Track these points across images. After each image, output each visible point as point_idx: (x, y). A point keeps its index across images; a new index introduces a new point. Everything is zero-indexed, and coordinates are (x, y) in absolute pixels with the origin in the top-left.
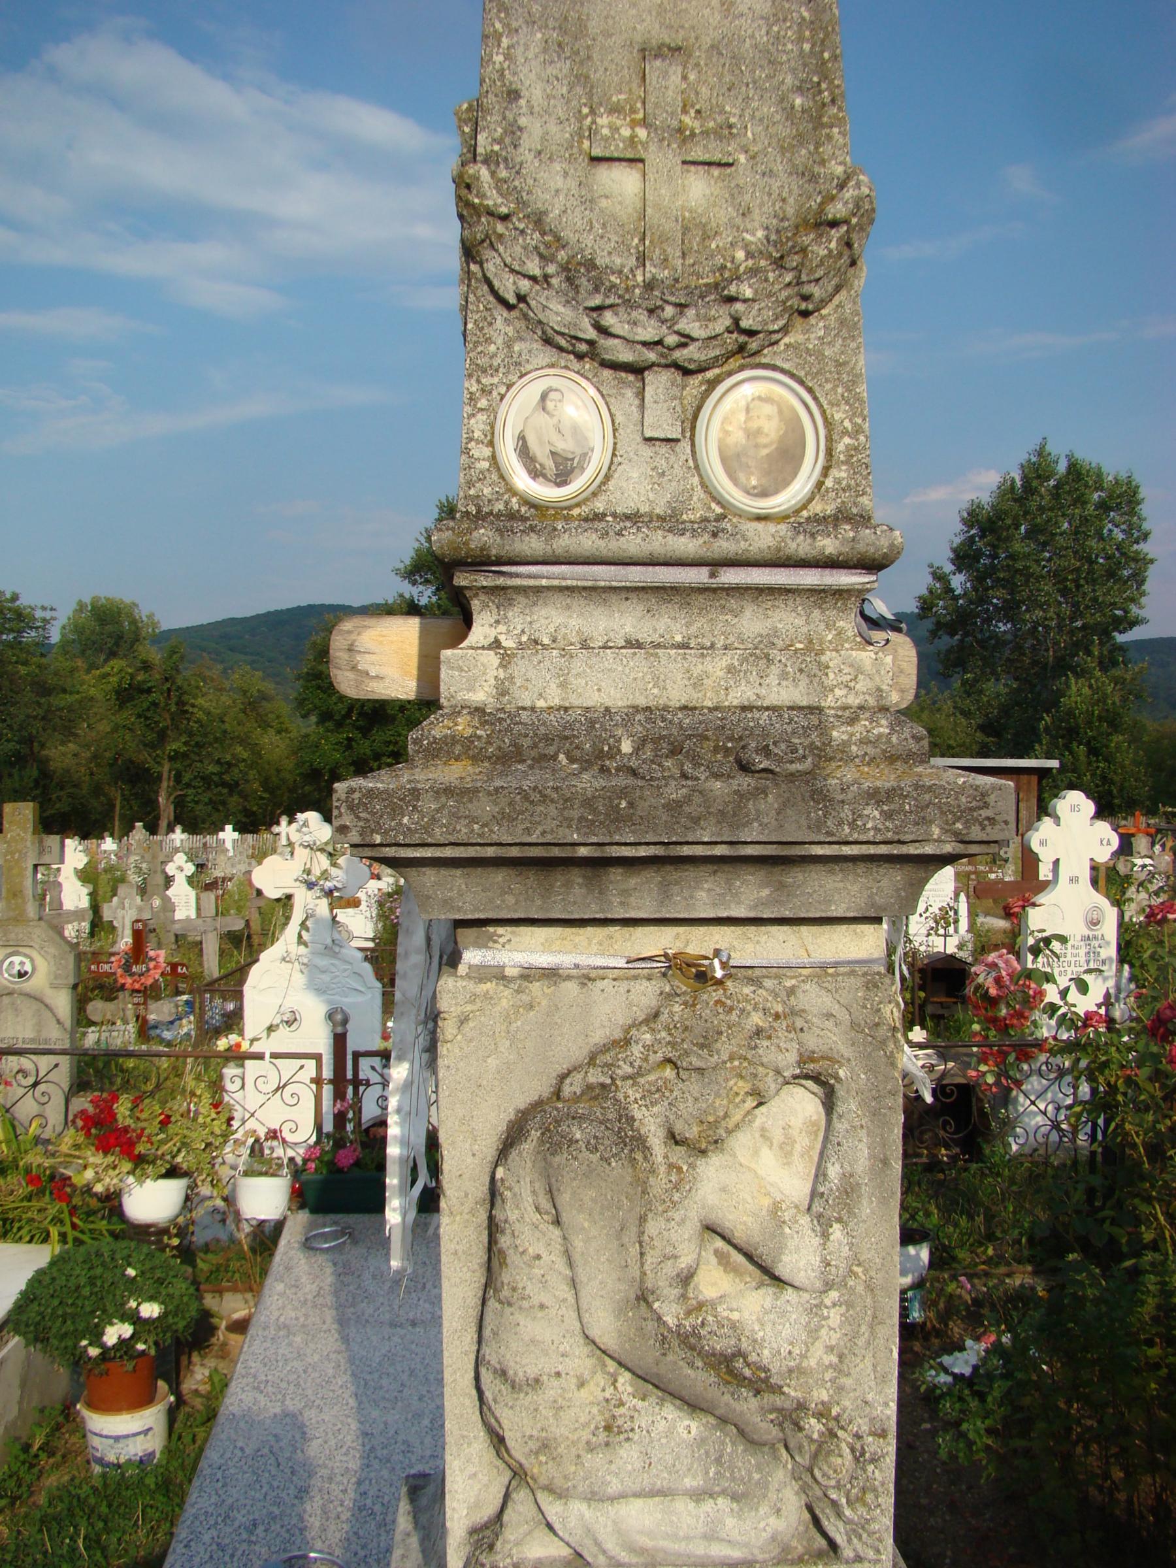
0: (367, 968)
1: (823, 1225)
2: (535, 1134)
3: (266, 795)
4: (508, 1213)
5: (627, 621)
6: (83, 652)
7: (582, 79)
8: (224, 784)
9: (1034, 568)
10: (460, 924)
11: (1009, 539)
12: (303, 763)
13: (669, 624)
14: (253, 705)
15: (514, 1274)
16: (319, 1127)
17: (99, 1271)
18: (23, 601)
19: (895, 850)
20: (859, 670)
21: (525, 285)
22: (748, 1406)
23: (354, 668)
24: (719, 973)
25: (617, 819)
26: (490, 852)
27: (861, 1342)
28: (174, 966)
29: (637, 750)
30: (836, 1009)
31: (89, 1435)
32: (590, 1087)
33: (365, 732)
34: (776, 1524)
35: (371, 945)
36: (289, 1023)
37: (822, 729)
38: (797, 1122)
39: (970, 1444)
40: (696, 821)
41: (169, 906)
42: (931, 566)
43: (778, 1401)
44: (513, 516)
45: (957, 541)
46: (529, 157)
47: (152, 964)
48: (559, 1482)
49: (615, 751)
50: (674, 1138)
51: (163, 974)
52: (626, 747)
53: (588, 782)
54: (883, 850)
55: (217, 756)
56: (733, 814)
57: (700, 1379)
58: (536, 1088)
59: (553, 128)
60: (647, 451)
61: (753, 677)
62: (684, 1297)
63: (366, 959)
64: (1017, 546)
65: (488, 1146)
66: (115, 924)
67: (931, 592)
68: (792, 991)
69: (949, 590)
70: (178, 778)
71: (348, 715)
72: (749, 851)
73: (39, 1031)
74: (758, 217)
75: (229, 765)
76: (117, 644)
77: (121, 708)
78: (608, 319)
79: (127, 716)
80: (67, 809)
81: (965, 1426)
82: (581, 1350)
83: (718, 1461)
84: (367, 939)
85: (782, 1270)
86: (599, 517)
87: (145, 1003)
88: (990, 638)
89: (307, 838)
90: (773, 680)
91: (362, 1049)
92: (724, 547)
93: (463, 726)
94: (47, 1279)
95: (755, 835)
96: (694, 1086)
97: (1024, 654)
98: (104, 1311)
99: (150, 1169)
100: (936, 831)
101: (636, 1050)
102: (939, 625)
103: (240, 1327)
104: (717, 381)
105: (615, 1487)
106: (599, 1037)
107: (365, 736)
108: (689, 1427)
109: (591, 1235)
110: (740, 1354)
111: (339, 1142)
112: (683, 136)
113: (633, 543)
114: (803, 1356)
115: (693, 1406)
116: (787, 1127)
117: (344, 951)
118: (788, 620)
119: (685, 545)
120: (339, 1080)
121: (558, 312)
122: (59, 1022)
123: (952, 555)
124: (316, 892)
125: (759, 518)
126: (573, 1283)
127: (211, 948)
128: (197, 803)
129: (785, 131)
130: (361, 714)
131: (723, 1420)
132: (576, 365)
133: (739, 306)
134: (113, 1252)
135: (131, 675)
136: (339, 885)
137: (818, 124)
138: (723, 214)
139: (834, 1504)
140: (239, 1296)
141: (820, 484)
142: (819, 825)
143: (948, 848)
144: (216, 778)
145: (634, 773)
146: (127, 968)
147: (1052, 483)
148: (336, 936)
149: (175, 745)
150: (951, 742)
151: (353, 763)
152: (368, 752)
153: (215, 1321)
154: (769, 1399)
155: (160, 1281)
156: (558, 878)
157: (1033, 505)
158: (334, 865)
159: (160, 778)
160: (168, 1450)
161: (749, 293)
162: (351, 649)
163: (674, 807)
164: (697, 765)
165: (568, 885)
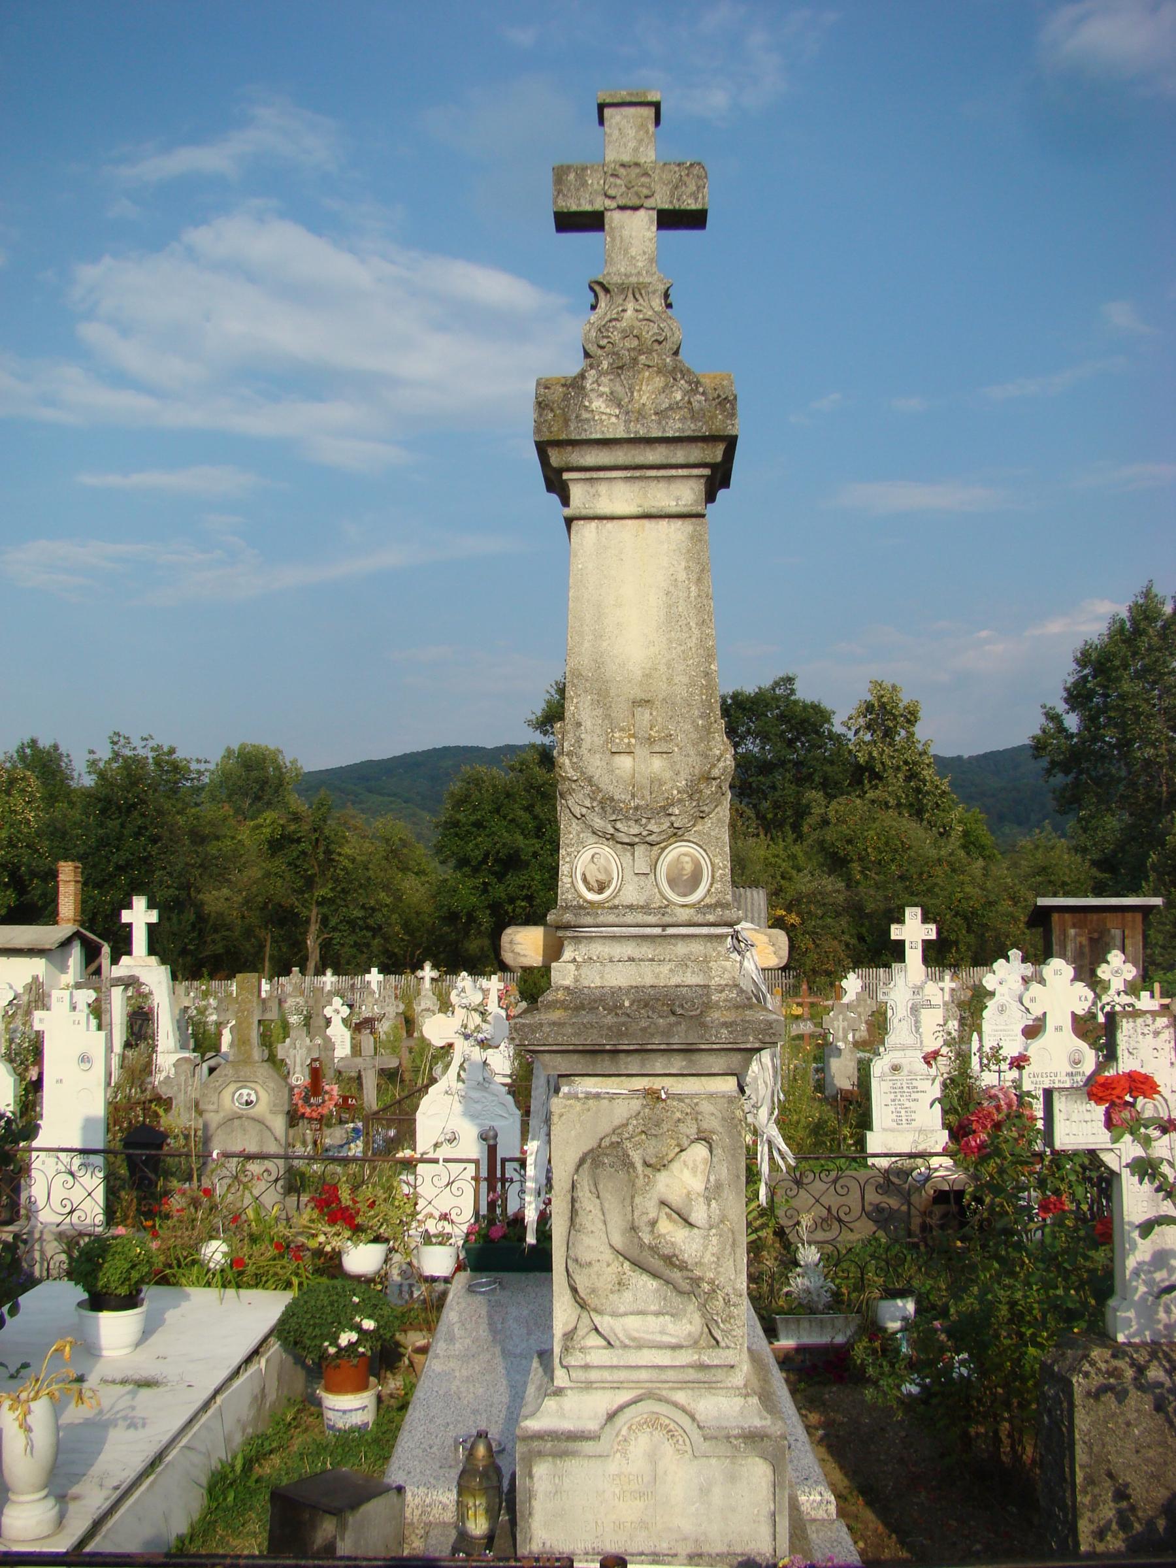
0: (510, 1098)
1: (708, 1200)
2: (589, 1161)
3: (406, 938)
4: (579, 1194)
5: (629, 949)
6: (230, 796)
7: (608, 716)
8: (368, 928)
9: (1144, 707)
10: (560, 1076)
11: (1119, 679)
12: (443, 906)
13: (647, 950)
14: (395, 855)
15: (581, 1219)
16: (476, 1213)
17: (335, 1297)
18: (179, 755)
19: (735, 1046)
20: (725, 970)
21: (584, 811)
22: (676, 1275)
23: (513, 951)
24: (664, 1096)
25: (620, 1034)
26: (571, 1048)
27: (727, 1252)
28: (345, 1099)
29: (631, 1004)
30: (715, 1112)
31: (325, 1411)
32: (612, 1143)
33: (500, 877)
34: (689, 1327)
35: (508, 1080)
36: (450, 1141)
37: (708, 995)
38: (699, 1159)
39: (885, 1394)
40: (652, 1035)
41: (329, 1045)
42: (1043, 707)
43: (690, 1274)
44: (581, 907)
45: (1071, 680)
46: (586, 752)
47: (327, 1097)
48: (599, 1306)
49: (622, 1006)
50: (646, 1164)
51: (336, 1105)
52: (627, 1004)
53: (610, 1020)
54: (730, 1046)
55: (362, 901)
56: (668, 1032)
57: (656, 1263)
58: (590, 1144)
59: (596, 739)
60: (636, 879)
61: (681, 973)
62: (652, 1232)
63: (509, 1093)
64: (1126, 687)
65: (571, 1167)
66: (287, 1061)
67: (1044, 732)
68: (697, 1104)
69: (1061, 729)
70: (325, 921)
71: (484, 861)
72: (675, 1047)
73: (261, 1146)
74: (683, 775)
75: (373, 909)
76: (262, 789)
77: (272, 856)
78: (619, 825)
79: (279, 864)
80: (221, 951)
81: (881, 1382)
82: (609, 1251)
83: (665, 1299)
84: (504, 1076)
85: (692, 1220)
86: (616, 907)
87: (320, 1129)
88: (1105, 775)
89: (464, 1001)
90: (688, 974)
91: (508, 1156)
92: (667, 919)
93: (560, 995)
94: (302, 1302)
95: (677, 1041)
96: (653, 1142)
97: (1138, 791)
98: (339, 1323)
99: (363, 1236)
100: (751, 1039)
101: (630, 1128)
102: (1053, 763)
103: (424, 1350)
104: (666, 847)
105: (622, 1310)
106: (617, 1122)
107: (500, 881)
108: (653, 1284)
109: (612, 1202)
110: (675, 1255)
111: (491, 1222)
112: (650, 741)
113: (629, 919)
114: (702, 1257)
115: (655, 1275)
116: (695, 1161)
117: (492, 1086)
118: (697, 948)
119: (651, 919)
120: (491, 1180)
121: (598, 823)
122: (276, 1139)
123: (1065, 695)
124: (472, 1041)
125: (683, 906)
126: (605, 1223)
127: (370, 1082)
128: (343, 945)
129: (694, 736)
130: (497, 860)
131: (667, 1282)
132: (606, 842)
133: (673, 818)
134: (344, 1287)
135: (282, 826)
136: (488, 1037)
137: (709, 733)
138: (668, 774)
139: (716, 1321)
140: (418, 1333)
141: (709, 891)
142: (702, 1037)
143: (757, 1045)
144: (360, 923)
145: (628, 1015)
146: (306, 1100)
147: (1159, 624)
148: (486, 1075)
149: (322, 892)
150: (1066, 879)
151: (489, 907)
152: (503, 896)
153: (402, 1350)
154: (685, 1273)
155: (375, 1306)
156: (599, 1057)
157: (1143, 644)
158: (484, 1021)
159: (308, 921)
160: (377, 1424)
161: (677, 812)
162: (511, 942)
163: (644, 1030)
164: (654, 1012)
165: (603, 1060)
